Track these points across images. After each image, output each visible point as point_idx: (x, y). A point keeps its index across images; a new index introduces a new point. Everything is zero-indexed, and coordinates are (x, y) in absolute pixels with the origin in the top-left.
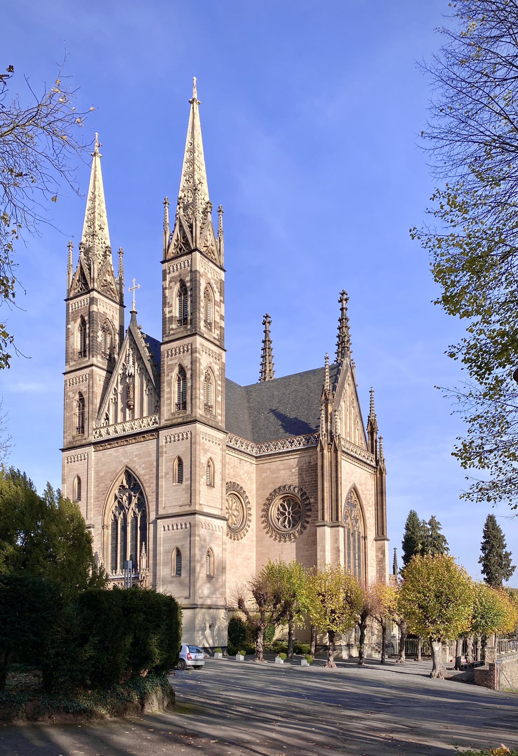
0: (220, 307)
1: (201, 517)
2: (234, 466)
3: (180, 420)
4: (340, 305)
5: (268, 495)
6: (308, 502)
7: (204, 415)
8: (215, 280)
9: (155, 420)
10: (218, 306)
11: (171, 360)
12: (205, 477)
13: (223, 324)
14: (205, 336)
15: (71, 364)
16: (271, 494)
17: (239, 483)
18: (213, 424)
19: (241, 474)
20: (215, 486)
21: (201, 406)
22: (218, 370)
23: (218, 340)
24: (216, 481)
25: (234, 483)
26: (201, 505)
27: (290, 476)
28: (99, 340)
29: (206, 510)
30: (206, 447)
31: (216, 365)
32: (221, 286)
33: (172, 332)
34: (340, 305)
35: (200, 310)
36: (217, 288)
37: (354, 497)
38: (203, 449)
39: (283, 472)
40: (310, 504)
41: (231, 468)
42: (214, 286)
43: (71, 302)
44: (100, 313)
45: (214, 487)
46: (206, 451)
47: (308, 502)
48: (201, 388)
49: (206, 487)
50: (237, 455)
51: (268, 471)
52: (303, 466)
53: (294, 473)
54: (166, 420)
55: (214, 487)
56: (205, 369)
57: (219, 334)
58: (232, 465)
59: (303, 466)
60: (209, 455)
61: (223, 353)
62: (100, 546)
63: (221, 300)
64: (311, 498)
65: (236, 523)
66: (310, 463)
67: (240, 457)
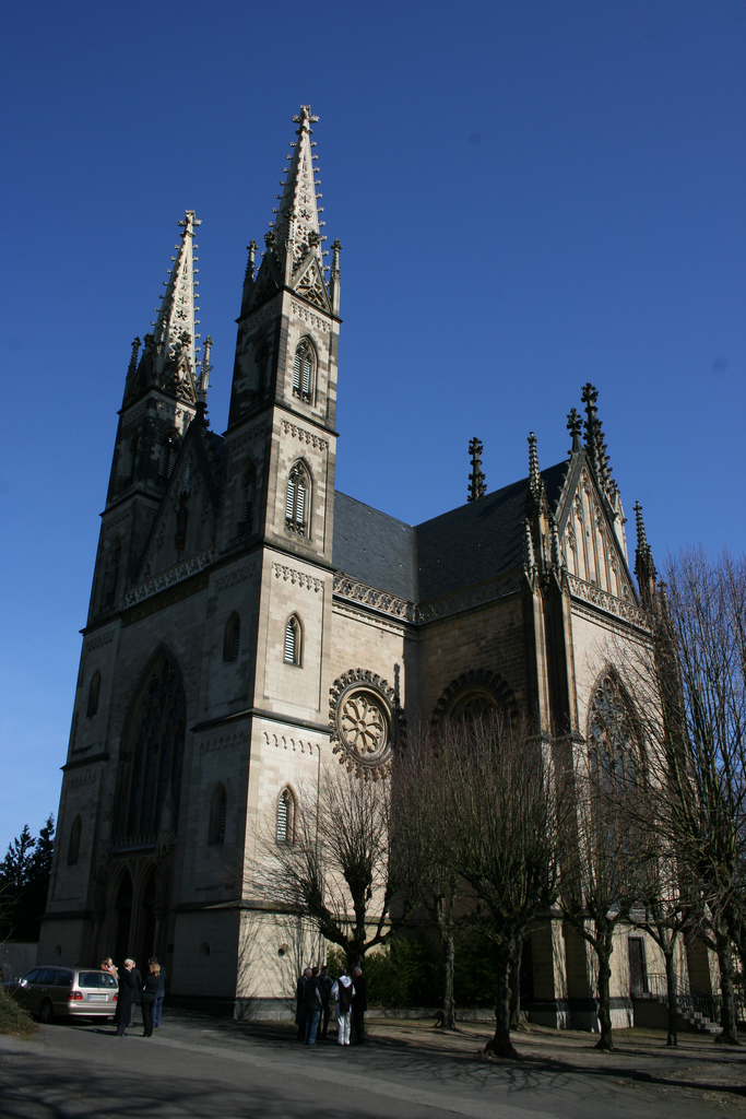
0: (329, 370)
1: (264, 722)
2: (368, 642)
3: (242, 547)
4: (585, 405)
5: (440, 693)
6: (511, 699)
7: (284, 535)
8: (320, 332)
9: (206, 557)
10: (324, 369)
11: (237, 454)
12: (280, 647)
13: (333, 395)
14: (294, 408)
15: (114, 498)
16: (447, 691)
17: (377, 673)
18: (305, 552)
19: (384, 657)
20: (304, 664)
21: (277, 520)
22: (319, 464)
23: (321, 418)
24: (306, 656)
25: (367, 672)
26: (266, 698)
27: (478, 655)
28: (154, 457)
29: (277, 709)
30: (285, 592)
31: (317, 457)
32: (331, 342)
33: (242, 413)
34: (585, 405)
35: (284, 370)
36: (324, 343)
37: (339, 495)
38: (276, 594)
39: (465, 648)
40: (514, 702)
41: (362, 644)
42: (320, 343)
43: (126, 413)
44: (160, 420)
45: (301, 666)
46: (284, 599)
47: (511, 699)
48: (279, 489)
49: (282, 665)
50: (373, 623)
51: (440, 651)
52: (499, 633)
53: (484, 647)
54: (221, 554)
55: (301, 666)
56: (289, 460)
57: (325, 409)
58: (363, 639)
59: (499, 633)
60: (291, 608)
61: (332, 440)
62: (257, 917)
63: (330, 361)
64: (517, 691)
65: (373, 748)
66: (512, 624)
67: (381, 625)
